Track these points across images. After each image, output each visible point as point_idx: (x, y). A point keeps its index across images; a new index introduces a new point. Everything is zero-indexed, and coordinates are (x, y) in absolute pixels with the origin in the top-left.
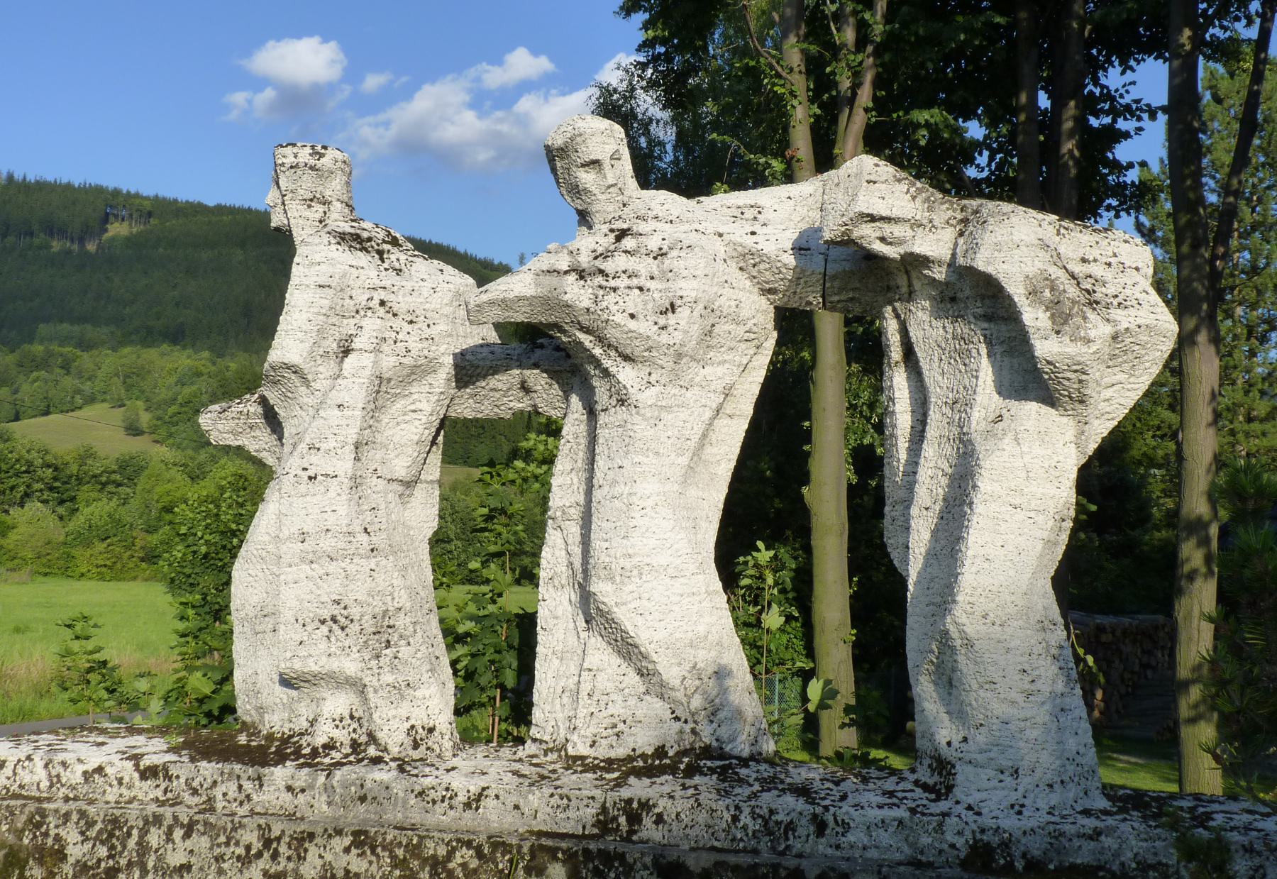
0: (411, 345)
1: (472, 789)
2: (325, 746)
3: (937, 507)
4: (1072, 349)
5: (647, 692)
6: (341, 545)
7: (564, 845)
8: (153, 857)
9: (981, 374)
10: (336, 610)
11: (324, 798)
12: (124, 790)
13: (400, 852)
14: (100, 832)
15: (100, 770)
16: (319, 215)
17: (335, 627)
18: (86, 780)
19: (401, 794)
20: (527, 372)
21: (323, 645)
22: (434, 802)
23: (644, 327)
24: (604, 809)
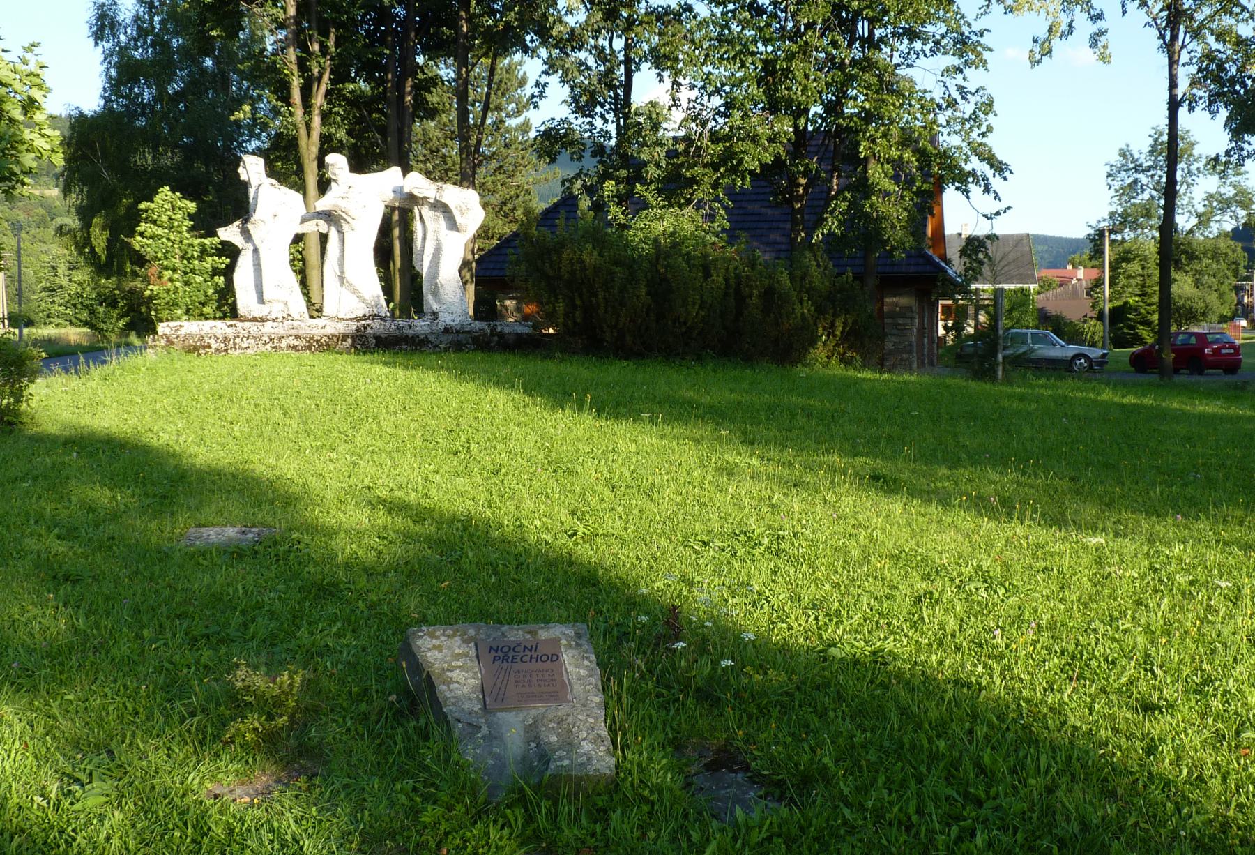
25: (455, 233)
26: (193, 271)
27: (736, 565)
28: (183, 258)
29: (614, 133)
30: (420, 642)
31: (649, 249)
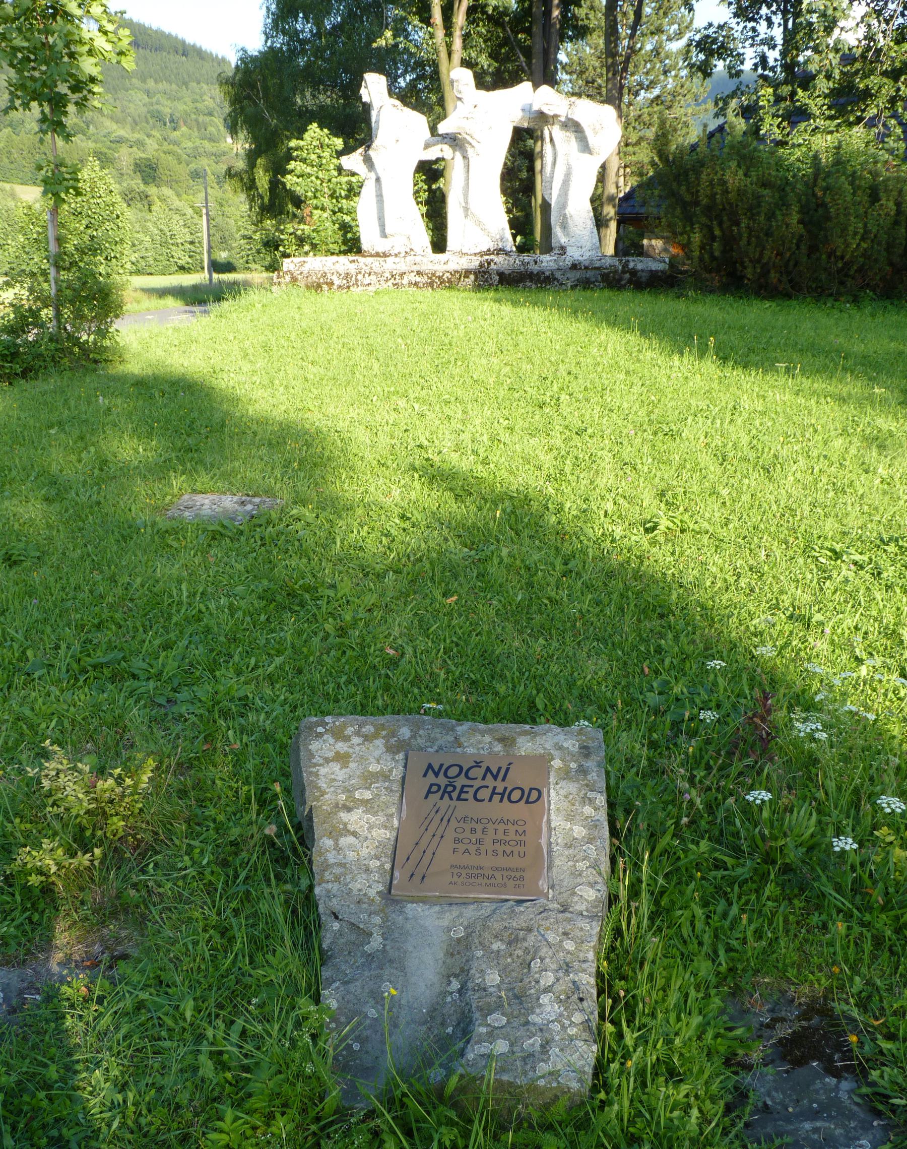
25: (587, 155)
27: (879, 596)
28: (332, 196)
29: (779, 40)
30: (314, 746)
31: (807, 170)
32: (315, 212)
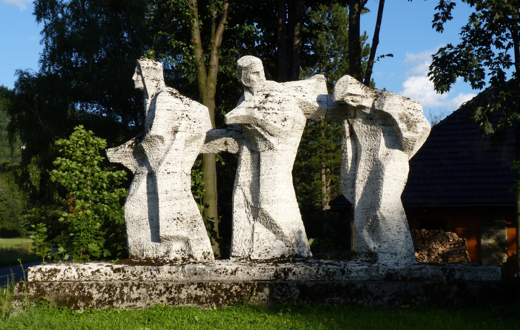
0: (195, 130)
1: (233, 269)
2: (174, 260)
3: (366, 180)
4: (413, 135)
5: (277, 239)
6: (179, 195)
7: (268, 282)
8: (126, 296)
9: (381, 141)
10: (179, 216)
11: (182, 274)
12: (107, 277)
13: (214, 288)
14: (105, 290)
15: (98, 271)
16: (156, 85)
17: (179, 221)
18: (93, 274)
19: (209, 272)
20: (228, 139)
21: (175, 227)
22: (220, 273)
23: (278, 125)
24: (276, 271)
26: (102, 201)
32: (78, 201)
